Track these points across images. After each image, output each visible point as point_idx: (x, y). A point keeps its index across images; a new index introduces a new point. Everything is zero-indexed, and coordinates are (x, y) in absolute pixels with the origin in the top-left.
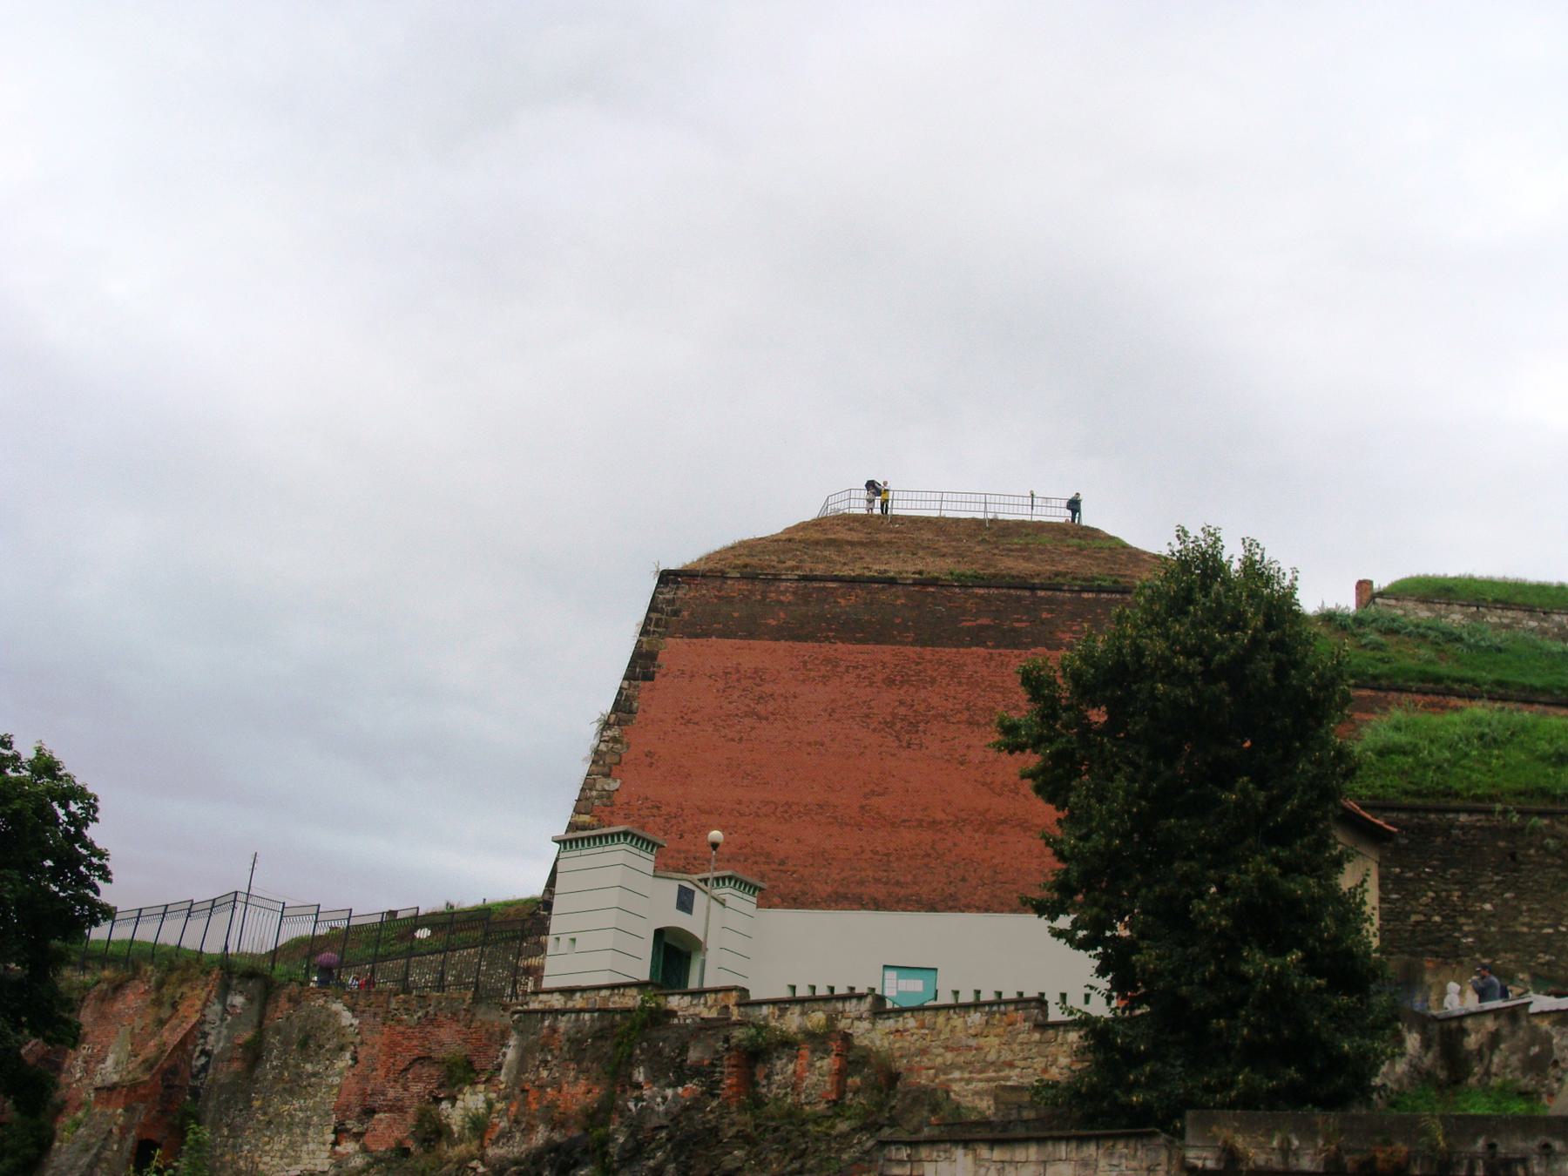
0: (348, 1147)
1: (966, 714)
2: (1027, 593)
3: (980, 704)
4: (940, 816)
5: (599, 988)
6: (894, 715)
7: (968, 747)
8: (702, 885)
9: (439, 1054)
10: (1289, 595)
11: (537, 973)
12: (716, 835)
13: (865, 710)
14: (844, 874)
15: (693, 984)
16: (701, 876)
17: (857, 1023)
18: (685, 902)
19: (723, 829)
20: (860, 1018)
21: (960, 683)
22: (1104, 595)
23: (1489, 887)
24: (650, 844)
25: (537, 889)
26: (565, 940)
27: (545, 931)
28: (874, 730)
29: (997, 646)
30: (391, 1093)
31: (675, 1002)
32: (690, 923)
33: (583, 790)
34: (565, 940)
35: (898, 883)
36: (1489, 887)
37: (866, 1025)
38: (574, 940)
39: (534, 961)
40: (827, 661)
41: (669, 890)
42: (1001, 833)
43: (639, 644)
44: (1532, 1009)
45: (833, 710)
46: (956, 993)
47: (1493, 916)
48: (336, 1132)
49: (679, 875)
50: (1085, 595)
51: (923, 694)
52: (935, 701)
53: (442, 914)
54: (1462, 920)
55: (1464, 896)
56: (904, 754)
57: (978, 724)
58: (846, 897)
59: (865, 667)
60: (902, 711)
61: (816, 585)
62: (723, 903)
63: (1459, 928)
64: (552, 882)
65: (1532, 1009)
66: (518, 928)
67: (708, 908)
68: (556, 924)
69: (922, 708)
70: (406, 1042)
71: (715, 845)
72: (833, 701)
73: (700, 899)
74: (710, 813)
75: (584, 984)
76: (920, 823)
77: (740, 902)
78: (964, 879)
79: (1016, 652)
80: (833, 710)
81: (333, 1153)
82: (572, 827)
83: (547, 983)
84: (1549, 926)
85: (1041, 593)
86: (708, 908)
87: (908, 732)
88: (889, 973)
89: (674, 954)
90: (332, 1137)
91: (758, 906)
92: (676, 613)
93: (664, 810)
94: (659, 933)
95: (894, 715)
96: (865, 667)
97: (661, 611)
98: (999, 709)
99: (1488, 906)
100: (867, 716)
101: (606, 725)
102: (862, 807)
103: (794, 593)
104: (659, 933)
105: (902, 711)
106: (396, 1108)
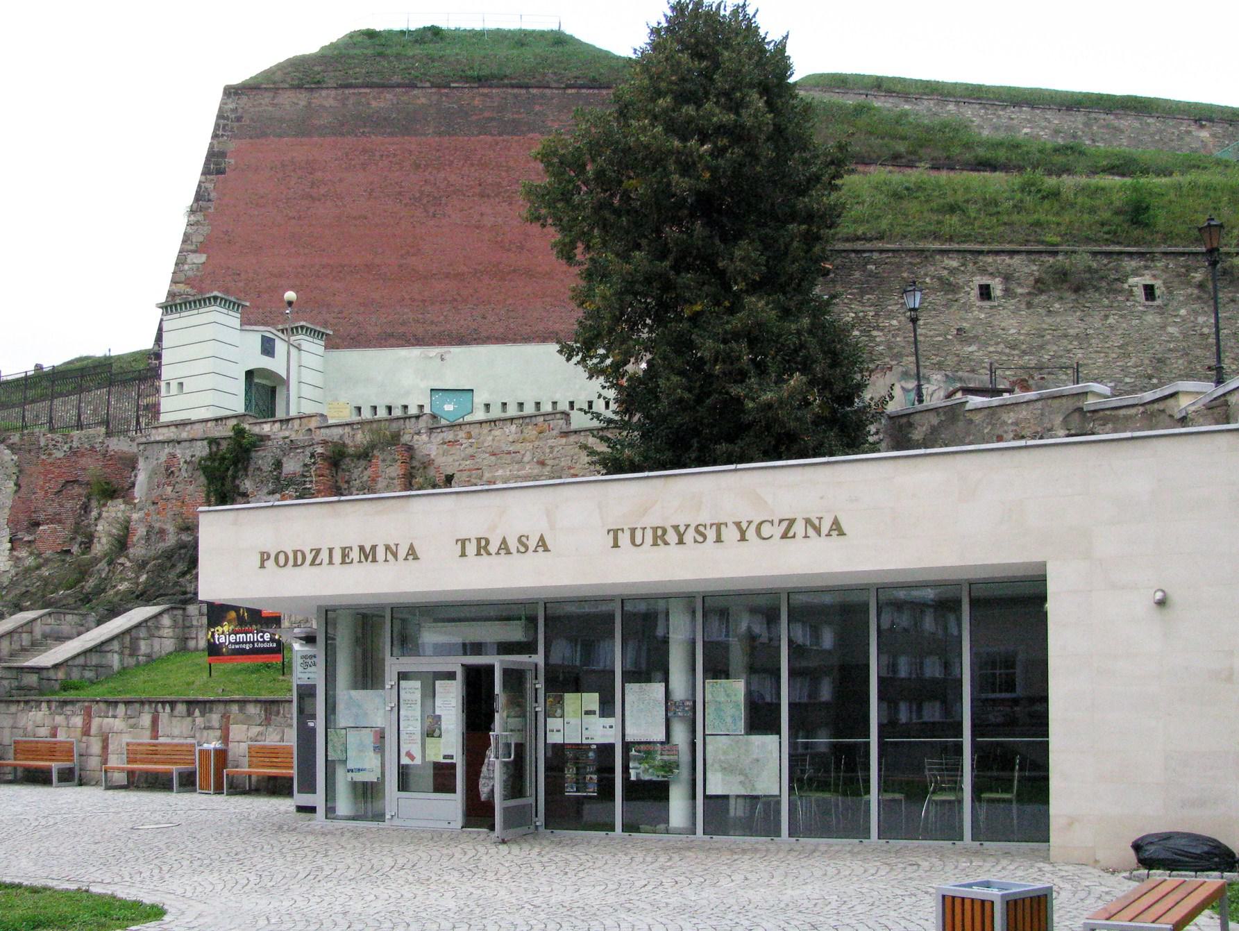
0: (23, 553)
1: (478, 190)
2: (523, 91)
3: (490, 181)
4: (463, 269)
5: (207, 421)
6: (422, 193)
7: (482, 215)
8: (280, 334)
9: (84, 478)
10: (777, 61)
11: (154, 410)
12: (290, 295)
13: (398, 189)
14: (390, 318)
15: (280, 414)
16: (280, 327)
17: (416, 437)
18: (268, 348)
19: (292, 288)
20: (419, 433)
21: (472, 165)
22: (584, 91)
23: (895, 308)
24: (236, 306)
25: (148, 344)
26: (174, 385)
27: (158, 377)
28: (406, 205)
29: (500, 134)
30: (50, 510)
31: (267, 428)
32: (276, 364)
33: (177, 264)
34: (174, 385)
35: (432, 323)
36: (895, 308)
37: (424, 437)
38: (181, 384)
39: (150, 400)
40: (364, 151)
41: (253, 340)
42: (511, 280)
43: (211, 146)
44: (968, 407)
45: (372, 190)
46: (421, 407)
47: (899, 329)
48: (11, 541)
49: (261, 328)
50: (569, 91)
51: (442, 175)
52: (452, 178)
53: (759, 45)
54: (875, 333)
55: (877, 315)
56: (432, 223)
57: (488, 196)
58: (392, 335)
59: (395, 155)
60: (428, 189)
61: (352, 91)
62: (299, 349)
63: (872, 339)
64: (159, 339)
65: (968, 407)
66: (139, 374)
67: (288, 353)
68: (166, 373)
69: (442, 186)
70: (57, 471)
71: (290, 303)
72: (372, 183)
73: (280, 347)
74: (280, 276)
75: (194, 418)
76: (447, 276)
77: (312, 348)
78: (484, 318)
79: (516, 138)
80: (372, 190)
81: (11, 557)
82: (171, 295)
83: (164, 418)
84: (940, 335)
85: (534, 91)
86: (288, 353)
87: (434, 205)
88: (436, 396)
89: (263, 390)
90: (9, 545)
91: (326, 348)
92: (239, 119)
93: (243, 276)
94: (250, 374)
95: (422, 193)
96: (395, 155)
97: (227, 118)
98: (505, 183)
99: (894, 322)
100: (400, 193)
101: (192, 211)
102: (401, 266)
103: (335, 99)
104: (250, 374)
105: (428, 189)
106: (55, 519)
